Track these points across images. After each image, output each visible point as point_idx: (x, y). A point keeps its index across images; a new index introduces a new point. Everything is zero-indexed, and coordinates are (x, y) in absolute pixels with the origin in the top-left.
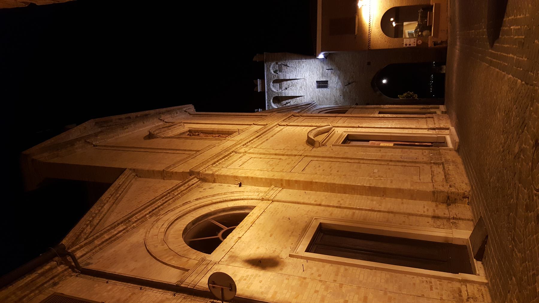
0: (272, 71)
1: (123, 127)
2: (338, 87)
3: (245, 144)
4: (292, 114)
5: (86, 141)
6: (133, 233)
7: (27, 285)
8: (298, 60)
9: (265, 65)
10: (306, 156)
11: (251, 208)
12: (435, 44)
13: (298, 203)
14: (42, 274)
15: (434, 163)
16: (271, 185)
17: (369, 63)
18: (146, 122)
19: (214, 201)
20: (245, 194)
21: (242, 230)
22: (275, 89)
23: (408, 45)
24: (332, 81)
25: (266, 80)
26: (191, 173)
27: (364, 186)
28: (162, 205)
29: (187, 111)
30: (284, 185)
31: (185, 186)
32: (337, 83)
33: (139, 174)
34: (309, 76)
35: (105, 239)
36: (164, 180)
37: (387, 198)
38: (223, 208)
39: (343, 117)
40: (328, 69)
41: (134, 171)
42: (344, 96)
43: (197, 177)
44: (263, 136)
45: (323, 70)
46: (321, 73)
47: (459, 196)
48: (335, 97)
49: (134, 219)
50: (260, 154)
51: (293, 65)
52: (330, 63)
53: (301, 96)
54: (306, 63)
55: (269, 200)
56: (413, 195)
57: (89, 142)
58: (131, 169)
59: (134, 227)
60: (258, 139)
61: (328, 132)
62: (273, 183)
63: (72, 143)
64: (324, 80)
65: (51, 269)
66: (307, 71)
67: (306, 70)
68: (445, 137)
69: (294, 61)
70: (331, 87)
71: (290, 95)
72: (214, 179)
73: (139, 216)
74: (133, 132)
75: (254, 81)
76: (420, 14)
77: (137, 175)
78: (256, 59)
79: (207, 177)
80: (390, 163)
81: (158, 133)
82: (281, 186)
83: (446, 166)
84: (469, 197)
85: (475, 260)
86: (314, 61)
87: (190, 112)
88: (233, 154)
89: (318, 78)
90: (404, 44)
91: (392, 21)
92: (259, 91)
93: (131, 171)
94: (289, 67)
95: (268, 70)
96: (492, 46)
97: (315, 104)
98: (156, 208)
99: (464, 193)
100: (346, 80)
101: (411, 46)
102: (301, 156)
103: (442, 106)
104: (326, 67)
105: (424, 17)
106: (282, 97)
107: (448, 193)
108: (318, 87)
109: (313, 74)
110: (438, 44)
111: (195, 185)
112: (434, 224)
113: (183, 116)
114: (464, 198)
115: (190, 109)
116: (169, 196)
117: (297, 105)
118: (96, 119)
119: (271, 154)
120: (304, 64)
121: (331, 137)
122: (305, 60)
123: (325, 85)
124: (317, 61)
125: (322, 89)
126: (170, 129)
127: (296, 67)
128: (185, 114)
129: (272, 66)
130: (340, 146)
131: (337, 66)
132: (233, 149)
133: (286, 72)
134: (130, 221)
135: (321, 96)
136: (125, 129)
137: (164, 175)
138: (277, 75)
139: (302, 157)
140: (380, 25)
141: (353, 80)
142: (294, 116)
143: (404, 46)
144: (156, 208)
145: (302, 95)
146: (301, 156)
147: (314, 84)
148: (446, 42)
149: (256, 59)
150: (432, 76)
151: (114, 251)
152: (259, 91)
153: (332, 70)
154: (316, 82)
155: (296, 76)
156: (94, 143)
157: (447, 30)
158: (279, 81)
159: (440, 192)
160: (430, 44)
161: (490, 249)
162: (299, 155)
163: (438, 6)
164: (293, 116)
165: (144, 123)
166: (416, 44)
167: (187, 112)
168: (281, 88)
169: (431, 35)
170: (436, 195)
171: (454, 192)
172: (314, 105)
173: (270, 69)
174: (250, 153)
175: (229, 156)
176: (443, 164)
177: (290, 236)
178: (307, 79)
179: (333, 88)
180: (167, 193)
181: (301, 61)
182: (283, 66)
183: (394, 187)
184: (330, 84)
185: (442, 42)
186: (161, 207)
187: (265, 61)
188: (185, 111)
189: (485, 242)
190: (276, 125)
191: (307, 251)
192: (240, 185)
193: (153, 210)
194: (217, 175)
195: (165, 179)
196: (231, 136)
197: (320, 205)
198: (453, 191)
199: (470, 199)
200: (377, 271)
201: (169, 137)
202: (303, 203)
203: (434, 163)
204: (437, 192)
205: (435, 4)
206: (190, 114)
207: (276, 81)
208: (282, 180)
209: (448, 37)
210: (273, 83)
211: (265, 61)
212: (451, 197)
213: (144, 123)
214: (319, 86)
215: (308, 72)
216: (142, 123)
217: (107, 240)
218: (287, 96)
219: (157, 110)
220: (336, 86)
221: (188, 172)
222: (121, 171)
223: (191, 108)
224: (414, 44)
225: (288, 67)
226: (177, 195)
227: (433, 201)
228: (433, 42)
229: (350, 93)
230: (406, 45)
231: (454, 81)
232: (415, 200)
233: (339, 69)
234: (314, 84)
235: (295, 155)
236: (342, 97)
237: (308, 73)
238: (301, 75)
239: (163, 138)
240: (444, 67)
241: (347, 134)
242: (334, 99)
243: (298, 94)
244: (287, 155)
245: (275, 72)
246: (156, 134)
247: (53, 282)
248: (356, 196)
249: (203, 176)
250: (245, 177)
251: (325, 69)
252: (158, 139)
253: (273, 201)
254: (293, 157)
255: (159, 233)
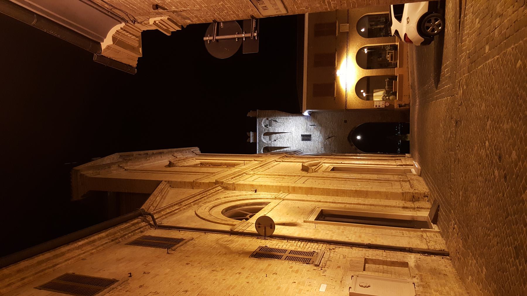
0: (263, 125)
1: (147, 158)
2: (320, 140)
3: (253, 170)
4: (285, 155)
5: (119, 166)
7: (125, 228)
8: (286, 116)
9: (258, 120)
10: (304, 176)
11: (266, 204)
12: (400, 106)
13: (303, 201)
14: (133, 225)
15: (402, 181)
16: (280, 191)
17: (346, 121)
18: (163, 156)
20: (261, 195)
22: (265, 140)
23: (378, 106)
24: (314, 135)
25: (257, 133)
26: (217, 183)
27: (352, 190)
28: (200, 199)
29: (194, 151)
30: (290, 191)
31: (213, 190)
32: (319, 137)
33: (172, 185)
34: (295, 130)
35: (167, 212)
36: (193, 189)
37: (369, 199)
38: (246, 203)
39: (327, 158)
40: (311, 125)
41: (169, 183)
42: (325, 148)
43: (220, 186)
44: (265, 166)
45: (307, 126)
46: (305, 128)
47: (421, 195)
48: (317, 149)
49: (183, 204)
50: (267, 175)
51: (281, 121)
52: (312, 120)
53: (288, 147)
54: (293, 119)
55: (280, 199)
56: (387, 196)
57: (121, 167)
58: (166, 181)
59: (184, 209)
60: (262, 168)
61: (316, 165)
62: (282, 189)
63: (109, 165)
64: (308, 134)
65: (138, 223)
66: (293, 126)
67: (292, 126)
68: (410, 169)
69: (282, 117)
70: (314, 141)
71: (278, 146)
72: (234, 187)
73: (186, 202)
74: (154, 163)
75: (247, 133)
76: (387, 83)
77: (170, 186)
78: (250, 114)
79: (229, 186)
80: (370, 181)
81: (177, 163)
82: (288, 191)
83: (411, 181)
84: (429, 196)
85: (432, 224)
86: (299, 118)
87: (196, 153)
88: (244, 174)
89: (303, 132)
90: (375, 105)
91: (363, 92)
92: (251, 142)
93: (166, 182)
94: (278, 122)
95: (260, 124)
96: (437, 87)
97: (302, 152)
98: (197, 200)
99: (425, 193)
100: (326, 134)
101: (381, 107)
102: (299, 176)
103: (408, 154)
104: (309, 123)
105: (390, 84)
106: (271, 147)
107: (413, 193)
108: (303, 140)
110: (402, 106)
111: (220, 191)
113: (191, 155)
114: (424, 196)
115: (196, 150)
116: (204, 195)
117: (287, 151)
118: (121, 153)
119: (275, 175)
120: (290, 121)
121: (319, 169)
122: (292, 117)
123: (308, 138)
124: (302, 118)
125: (306, 142)
126: (186, 161)
127: (284, 123)
128: (193, 154)
129: (263, 121)
130: (329, 172)
131: (319, 123)
132: (244, 171)
133: (275, 126)
134: (181, 205)
135: (306, 147)
136: (148, 160)
137: (193, 185)
138: (267, 128)
139: (300, 177)
140: (355, 90)
141: (332, 135)
142: (287, 157)
143: (375, 107)
144: (197, 200)
145: (289, 146)
146: (299, 176)
147: (299, 137)
148: (409, 105)
149: (250, 114)
150: (399, 150)
152: (251, 142)
153: (314, 126)
154: (301, 136)
155: (284, 130)
156: (125, 168)
157: (409, 95)
158: (269, 134)
159: (407, 193)
160: (396, 106)
161: (442, 214)
162: (298, 176)
163: (401, 76)
164: (285, 157)
165: (161, 157)
166: (384, 105)
167: (194, 152)
168: (270, 139)
169: (396, 99)
170: (404, 196)
171: (417, 192)
172: (300, 152)
173: (262, 124)
174: (258, 174)
175: (242, 176)
176: (409, 181)
177: (301, 214)
178: (293, 133)
179: (315, 141)
180: (202, 192)
181: (288, 117)
182: (273, 121)
183: (374, 190)
184: (313, 137)
185: (405, 105)
186: (200, 200)
187: (257, 116)
188: (192, 152)
189: (438, 210)
190: (273, 161)
191: (315, 220)
192: (256, 192)
193: (195, 201)
194: (237, 184)
195: (194, 188)
196: (238, 166)
197: (320, 201)
198: (416, 192)
199: (429, 197)
200: (366, 228)
201: (187, 166)
202: (307, 201)
203: (402, 181)
204: (405, 193)
205: (399, 75)
206: (197, 155)
207: (266, 134)
208: (288, 187)
209: (410, 101)
210: (263, 135)
211: (257, 116)
212: (416, 197)
213: (161, 157)
214: (304, 139)
215: (294, 127)
216: (160, 157)
217: (169, 213)
218: (276, 146)
219: (170, 149)
220: (318, 139)
221: (214, 182)
222: (158, 183)
223: (197, 150)
224: (383, 105)
225: (277, 123)
226: (209, 195)
227: (402, 200)
228: (398, 104)
229: (330, 145)
230: (376, 106)
231: (416, 129)
232: (390, 199)
233: (321, 125)
234: (299, 137)
235: (295, 176)
236: (323, 149)
237: (294, 128)
238: (288, 129)
239: (181, 167)
240: (409, 135)
241: (333, 167)
242: (316, 150)
243: (285, 145)
244: (288, 176)
245: (265, 126)
246: (175, 163)
247: (140, 231)
248: (345, 198)
249: (225, 185)
250: (260, 185)
251: (308, 125)
252: (176, 167)
253: (283, 200)
254: (293, 177)
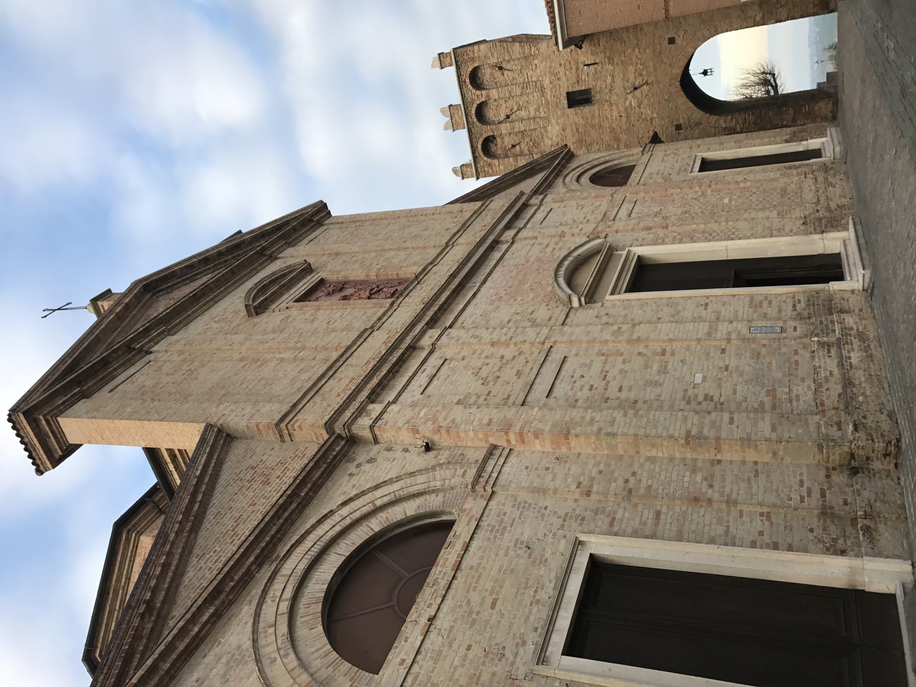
6: (230, 619)
19: (379, 503)
21: (435, 595)
109: (558, 79)
112: (824, 535)
151: (197, 681)
212: (859, 456)
255: (278, 616)
